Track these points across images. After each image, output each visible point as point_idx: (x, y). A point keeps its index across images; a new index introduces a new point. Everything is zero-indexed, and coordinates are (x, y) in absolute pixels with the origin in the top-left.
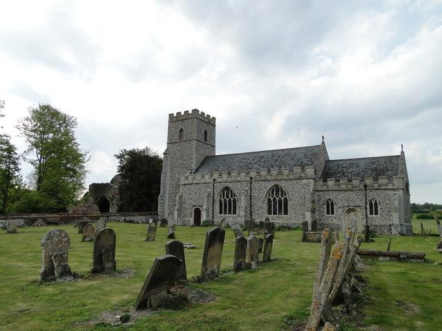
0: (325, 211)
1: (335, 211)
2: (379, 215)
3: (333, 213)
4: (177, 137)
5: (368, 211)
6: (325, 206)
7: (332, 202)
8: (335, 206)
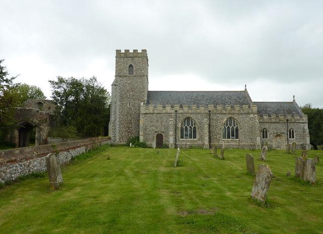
3: (266, 137)
4: (126, 71)
8: (268, 132)
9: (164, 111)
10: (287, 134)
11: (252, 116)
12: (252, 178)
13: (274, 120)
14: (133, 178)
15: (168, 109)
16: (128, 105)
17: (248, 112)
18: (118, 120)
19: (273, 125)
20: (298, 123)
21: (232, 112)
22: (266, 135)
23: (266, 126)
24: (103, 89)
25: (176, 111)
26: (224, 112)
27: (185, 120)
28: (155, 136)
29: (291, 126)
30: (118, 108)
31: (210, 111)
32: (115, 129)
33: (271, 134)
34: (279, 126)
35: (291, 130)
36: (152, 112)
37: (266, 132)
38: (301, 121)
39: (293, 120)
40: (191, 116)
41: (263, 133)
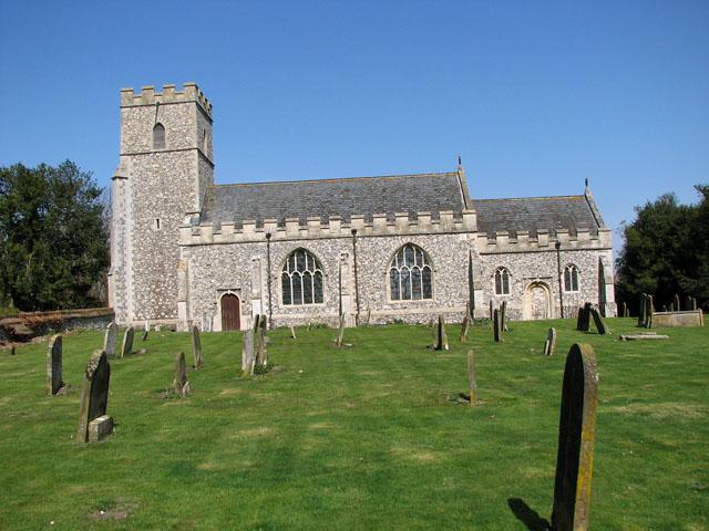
0: (494, 288)
1: (510, 287)
2: (579, 291)
5: (563, 285)
6: (493, 280)
8: (510, 278)
9: (239, 237)
10: (560, 280)
13: (523, 246)
18: (130, 263)
20: (587, 250)
21: (413, 229)
22: (506, 283)
23: (506, 261)
26: (391, 230)
27: (292, 256)
28: (219, 301)
29: (567, 258)
31: (354, 232)
33: (518, 281)
34: (537, 259)
35: (571, 270)
36: (208, 241)
37: (574, 273)
40: (308, 245)
41: (498, 279)
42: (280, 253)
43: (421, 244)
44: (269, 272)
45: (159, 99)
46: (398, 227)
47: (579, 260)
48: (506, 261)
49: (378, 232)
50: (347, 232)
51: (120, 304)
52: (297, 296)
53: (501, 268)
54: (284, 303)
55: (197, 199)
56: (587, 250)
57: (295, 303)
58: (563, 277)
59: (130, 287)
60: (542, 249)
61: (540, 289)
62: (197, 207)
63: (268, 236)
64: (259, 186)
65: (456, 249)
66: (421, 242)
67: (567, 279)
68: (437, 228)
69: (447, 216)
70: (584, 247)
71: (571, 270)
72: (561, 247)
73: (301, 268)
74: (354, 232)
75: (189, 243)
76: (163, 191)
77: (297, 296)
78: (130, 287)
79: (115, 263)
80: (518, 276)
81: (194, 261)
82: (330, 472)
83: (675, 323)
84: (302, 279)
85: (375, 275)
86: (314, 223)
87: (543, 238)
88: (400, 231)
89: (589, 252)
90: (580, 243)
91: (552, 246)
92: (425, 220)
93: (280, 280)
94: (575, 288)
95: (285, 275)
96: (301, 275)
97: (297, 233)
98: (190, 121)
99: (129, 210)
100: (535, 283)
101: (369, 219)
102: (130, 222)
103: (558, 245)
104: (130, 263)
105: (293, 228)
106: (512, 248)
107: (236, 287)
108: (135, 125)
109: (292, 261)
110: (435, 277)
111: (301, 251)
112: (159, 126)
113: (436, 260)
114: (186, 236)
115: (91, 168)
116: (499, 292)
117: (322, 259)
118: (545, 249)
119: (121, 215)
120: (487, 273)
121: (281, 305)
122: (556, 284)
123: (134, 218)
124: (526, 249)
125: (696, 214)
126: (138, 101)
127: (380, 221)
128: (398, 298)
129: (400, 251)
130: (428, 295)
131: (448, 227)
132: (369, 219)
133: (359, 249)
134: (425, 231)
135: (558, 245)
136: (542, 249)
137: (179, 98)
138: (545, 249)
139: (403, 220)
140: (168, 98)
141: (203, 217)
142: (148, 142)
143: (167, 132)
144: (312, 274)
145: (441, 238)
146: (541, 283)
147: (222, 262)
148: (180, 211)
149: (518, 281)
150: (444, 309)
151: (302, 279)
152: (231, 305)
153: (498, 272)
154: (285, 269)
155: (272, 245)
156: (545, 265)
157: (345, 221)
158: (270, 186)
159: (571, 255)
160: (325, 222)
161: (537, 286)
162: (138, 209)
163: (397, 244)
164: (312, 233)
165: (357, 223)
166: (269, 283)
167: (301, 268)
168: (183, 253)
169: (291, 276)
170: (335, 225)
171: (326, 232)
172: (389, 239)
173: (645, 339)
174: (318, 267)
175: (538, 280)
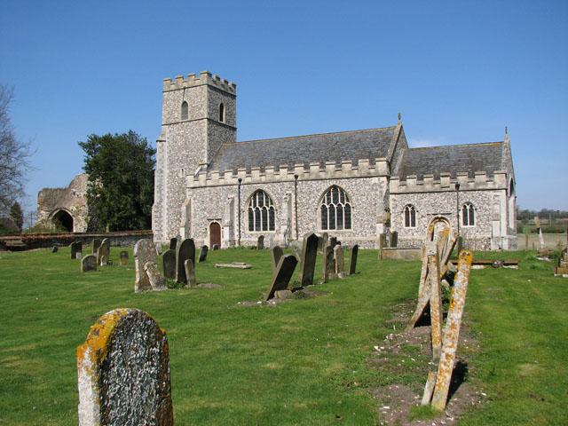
0: (404, 222)
1: (417, 221)
2: (475, 226)
5: (461, 221)
6: (403, 215)
7: (413, 208)
9: (222, 182)
10: (458, 216)
11: (375, 180)
12: (454, 306)
13: (428, 187)
14: (34, 276)
15: (228, 176)
16: (180, 175)
17: (369, 173)
18: (166, 200)
19: (427, 198)
20: (483, 190)
21: (338, 174)
22: (414, 218)
23: (413, 200)
24: (86, 168)
25: (240, 180)
26: (323, 175)
27: (254, 195)
28: (208, 228)
29: (466, 197)
30: (166, 180)
32: (161, 217)
33: (423, 216)
34: (440, 198)
35: (468, 207)
36: (203, 185)
37: (471, 211)
38: (490, 186)
39: (472, 185)
40: (264, 187)
41: (407, 213)
42: (247, 192)
43: (343, 186)
44: (239, 207)
45: (185, 85)
46: (327, 173)
47: (475, 199)
48: (413, 200)
49: (313, 177)
50: (292, 177)
51: (157, 228)
52: (258, 225)
53: (410, 205)
54: (323, 229)
55: (206, 155)
56: (483, 190)
57: (257, 230)
58: (461, 214)
59: (165, 217)
60: (444, 189)
61: (442, 223)
62: (205, 160)
63: (240, 180)
64: (254, 142)
65: (370, 191)
66: (343, 184)
67: (465, 215)
68: (356, 173)
69: (364, 164)
70: (481, 187)
71: (468, 207)
72: (461, 188)
73: (261, 204)
74: (296, 177)
75: (192, 186)
76: (186, 149)
77: (258, 225)
78: (165, 217)
79: (156, 199)
80: (423, 212)
81: (195, 199)
82: (40, 349)
83: (399, 257)
84: (262, 216)
85: (309, 210)
86: (270, 171)
87: (445, 181)
88: (329, 176)
89: (486, 192)
90: (478, 184)
91: (453, 187)
92: (347, 167)
93: (247, 213)
94: (472, 223)
95: (250, 209)
96: (335, 206)
97: (259, 179)
98: (203, 99)
99: (166, 163)
100: (437, 218)
101: (307, 167)
102: (166, 171)
103: (457, 186)
104: (166, 200)
105: (256, 174)
106: (419, 189)
107: (219, 218)
108: (171, 104)
109: (329, 195)
110: (353, 212)
111: (260, 192)
112: (185, 104)
113: (354, 198)
114: (190, 182)
115: (145, 134)
116: (407, 225)
117: (274, 198)
118: (446, 189)
119: (160, 167)
120: (399, 209)
121: (248, 232)
122: (455, 219)
123: (168, 169)
124: (431, 190)
125: (99, 183)
126: (173, 87)
127: (315, 169)
128: (252, 230)
129: (328, 192)
130: (348, 226)
131: (364, 172)
132: (307, 167)
133: (299, 190)
134: (347, 175)
135: (457, 186)
136: (444, 189)
137: (198, 82)
138: (446, 189)
139: (331, 167)
140: (191, 83)
141: (210, 166)
142: (178, 115)
143: (189, 107)
144: (343, 206)
145: (358, 180)
146: (442, 218)
147: (211, 199)
148: (196, 163)
149: (423, 216)
150: (359, 238)
151: (262, 216)
152: (215, 230)
153: (407, 209)
154: (250, 205)
155: (242, 187)
156: (446, 203)
157: (291, 169)
158: (260, 142)
159: (469, 195)
160: (277, 170)
161: (440, 221)
162: (171, 163)
163: (325, 186)
164: (269, 178)
165: (299, 170)
166: (239, 215)
167: (261, 204)
168: (188, 193)
169: (328, 207)
170: (283, 172)
171: (277, 177)
172: (320, 182)
173: (226, 268)
174: (272, 204)
175: (440, 216)
